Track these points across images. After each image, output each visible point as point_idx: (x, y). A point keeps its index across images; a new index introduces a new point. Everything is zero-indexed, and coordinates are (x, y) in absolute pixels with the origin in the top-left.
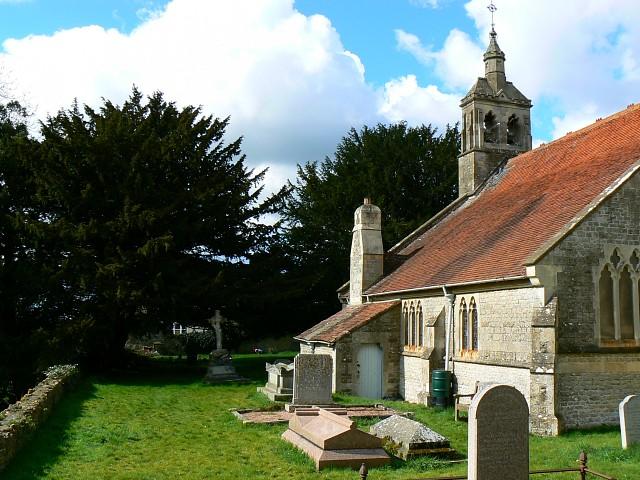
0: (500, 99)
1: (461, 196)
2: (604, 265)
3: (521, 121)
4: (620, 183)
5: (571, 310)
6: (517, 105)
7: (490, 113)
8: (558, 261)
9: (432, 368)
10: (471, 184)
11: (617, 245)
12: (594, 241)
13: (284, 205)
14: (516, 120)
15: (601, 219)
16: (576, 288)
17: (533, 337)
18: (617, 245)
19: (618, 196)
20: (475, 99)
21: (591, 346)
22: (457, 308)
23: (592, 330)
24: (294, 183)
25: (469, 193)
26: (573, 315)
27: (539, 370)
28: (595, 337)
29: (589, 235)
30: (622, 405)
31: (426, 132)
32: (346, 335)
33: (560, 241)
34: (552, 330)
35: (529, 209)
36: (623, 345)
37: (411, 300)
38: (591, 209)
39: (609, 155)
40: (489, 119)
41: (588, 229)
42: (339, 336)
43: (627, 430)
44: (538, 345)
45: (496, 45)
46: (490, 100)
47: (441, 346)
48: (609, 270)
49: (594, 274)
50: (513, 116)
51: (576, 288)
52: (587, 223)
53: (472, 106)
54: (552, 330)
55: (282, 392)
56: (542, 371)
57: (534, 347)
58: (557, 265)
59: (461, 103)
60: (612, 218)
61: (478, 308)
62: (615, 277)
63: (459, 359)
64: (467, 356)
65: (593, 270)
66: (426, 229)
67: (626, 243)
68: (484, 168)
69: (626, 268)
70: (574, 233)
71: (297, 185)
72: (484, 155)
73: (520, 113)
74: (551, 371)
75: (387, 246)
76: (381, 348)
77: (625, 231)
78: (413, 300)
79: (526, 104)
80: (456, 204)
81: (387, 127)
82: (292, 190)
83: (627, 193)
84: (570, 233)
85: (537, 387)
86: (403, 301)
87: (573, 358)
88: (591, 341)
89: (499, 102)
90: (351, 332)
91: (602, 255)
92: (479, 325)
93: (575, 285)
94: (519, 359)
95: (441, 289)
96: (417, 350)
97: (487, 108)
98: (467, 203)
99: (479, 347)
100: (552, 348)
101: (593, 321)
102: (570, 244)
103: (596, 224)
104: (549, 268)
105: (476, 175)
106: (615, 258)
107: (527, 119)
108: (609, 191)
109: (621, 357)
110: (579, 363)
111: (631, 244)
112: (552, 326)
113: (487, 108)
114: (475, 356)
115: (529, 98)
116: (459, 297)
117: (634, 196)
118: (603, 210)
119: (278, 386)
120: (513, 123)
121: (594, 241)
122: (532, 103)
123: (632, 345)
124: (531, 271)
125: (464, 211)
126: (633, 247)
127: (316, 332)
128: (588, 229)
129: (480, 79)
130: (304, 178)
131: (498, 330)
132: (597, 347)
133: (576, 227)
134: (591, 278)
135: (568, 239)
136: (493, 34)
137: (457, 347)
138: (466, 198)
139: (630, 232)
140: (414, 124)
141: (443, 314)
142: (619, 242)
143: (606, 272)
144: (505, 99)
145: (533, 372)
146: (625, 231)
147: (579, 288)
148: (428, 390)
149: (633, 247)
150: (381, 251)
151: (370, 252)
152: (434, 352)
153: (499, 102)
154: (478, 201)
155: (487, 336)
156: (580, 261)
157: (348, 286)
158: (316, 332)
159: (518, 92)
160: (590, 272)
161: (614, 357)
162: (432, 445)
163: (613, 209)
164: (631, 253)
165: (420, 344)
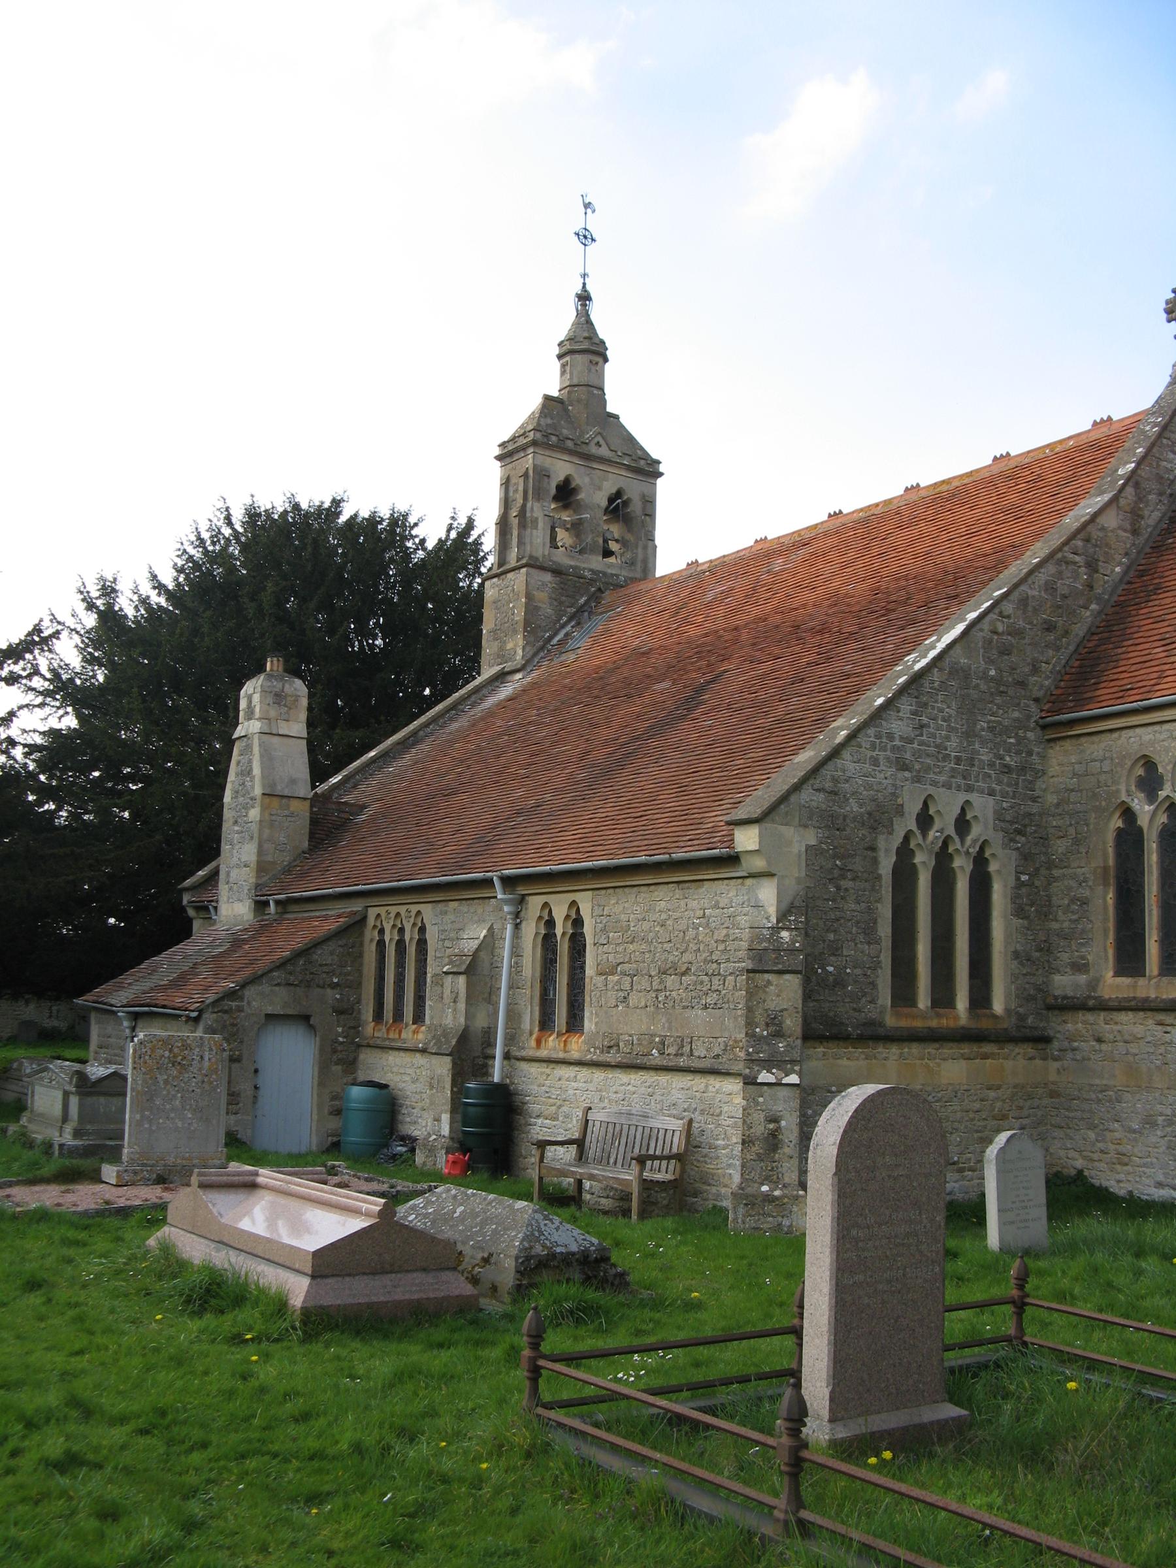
0: (594, 450)
1: (487, 672)
2: (902, 834)
3: (636, 507)
4: (940, 646)
5: (831, 936)
6: (628, 468)
7: (567, 480)
8: (812, 816)
9: (458, 1076)
10: (517, 646)
11: (931, 790)
12: (885, 775)
13: (36, 672)
14: (626, 503)
15: (898, 726)
16: (845, 884)
17: (750, 995)
18: (931, 790)
19: (936, 675)
20: (534, 443)
21: (871, 1023)
22: (531, 930)
23: (873, 985)
24: (64, 616)
25: (509, 666)
26: (835, 950)
27: (764, 1077)
28: (880, 1002)
29: (875, 762)
30: (992, 1151)
31: (399, 524)
32: (231, 995)
33: (815, 771)
34: (448, 1059)
35: (691, 701)
36: (934, 1023)
37: (394, 910)
38: (880, 701)
39: (876, 591)
40: (566, 493)
41: (873, 747)
42: (211, 997)
43: (1001, 1211)
44: (759, 1018)
45: (589, 322)
46: (571, 452)
47: (481, 1022)
48: (912, 846)
49: (881, 855)
50: (619, 494)
51: (845, 884)
52: (871, 731)
53: (528, 461)
54: (448, 1059)
55: (77, 1134)
56: (771, 1079)
57: (750, 1024)
58: (806, 826)
59: (497, 451)
60: (922, 726)
61: (588, 929)
62: (923, 861)
63: (530, 1053)
64: (552, 1045)
65: (881, 843)
66: (404, 745)
67: (947, 786)
68: (547, 610)
69: (945, 844)
70: (846, 754)
71: (71, 622)
72: (548, 577)
73: (633, 488)
74: (794, 1079)
75: (318, 773)
76: (312, 1028)
77: (946, 757)
78: (402, 910)
79: (648, 469)
80: (477, 690)
81: (304, 506)
82: (56, 635)
83: (955, 671)
84: (835, 753)
85: (758, 1117)
86: (372, 913)
87: (833, 1049)
88: (871, 1012)
89: (588, 457)
90: (243, 986)
91: (900, 811)
92: (590, 971)
93: (843, 877)
94: (700, 1051)
95: (488, 883)
96: (407, 1034)
97: (561, 468)
98: (506, 691)
99: (589, 1025)
100: (792, 1024)
101: (876, 966)
102: (835, 780)
103: (891, 737)
104: (788, 832)
105: (531, 626)
106: (925, 820)
107: (649, 503)
108: (918, 662)
109: (930, 1049)
110: (845, 1062)
111: (959, 788)
112: (447, 1055)
113: (561, 468)
114: (576, 1047)
115: (655, 456)
116: (535, 904)
117: (967, 677)
118: (906, 706)
119: (65, 1118)
120: (617, 507)
121: (885, 775)
122: (662, 468)
123: (952, 1024)
124: (747, 840)
125: (502, 705)
126: (962, 797)
127: (136, 988)
128: (873, 747)
129: (548, 399)
130: (91, 606)
131: (645, 983)
132: (881, 1024)
133: (851, 737)
134: (875, 862)
135: (830, 765)
136: (584, 298)
137: (526, 1025)
138: (501, 677)
139: (958, 760)
140: (357, 506)
141: (490, 943)
142: (934, 783)
143: (905, 852)
144: (604, 451)
145: (750, 1081)
146: (946, 757)
147: (850, 884)
148: (446, 1130)
149: (962, 797)
150: (303, 789)
151: (279, 789)
152: (464, 1037)
153: (588, 457)
154: (534, 685)
155: (612, 997)
156: (854, 819)
157: (216, 873)
158: (136, 988)
159: (630, 440)
160: (873, 849)
161: (915, 1049)
162: (567, 1260)
163: (925, 705)
164: (957, 811)
165: (419, 1018)
